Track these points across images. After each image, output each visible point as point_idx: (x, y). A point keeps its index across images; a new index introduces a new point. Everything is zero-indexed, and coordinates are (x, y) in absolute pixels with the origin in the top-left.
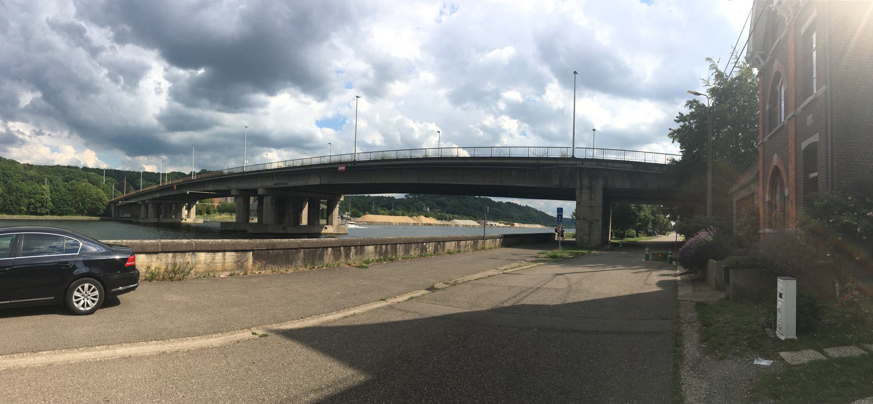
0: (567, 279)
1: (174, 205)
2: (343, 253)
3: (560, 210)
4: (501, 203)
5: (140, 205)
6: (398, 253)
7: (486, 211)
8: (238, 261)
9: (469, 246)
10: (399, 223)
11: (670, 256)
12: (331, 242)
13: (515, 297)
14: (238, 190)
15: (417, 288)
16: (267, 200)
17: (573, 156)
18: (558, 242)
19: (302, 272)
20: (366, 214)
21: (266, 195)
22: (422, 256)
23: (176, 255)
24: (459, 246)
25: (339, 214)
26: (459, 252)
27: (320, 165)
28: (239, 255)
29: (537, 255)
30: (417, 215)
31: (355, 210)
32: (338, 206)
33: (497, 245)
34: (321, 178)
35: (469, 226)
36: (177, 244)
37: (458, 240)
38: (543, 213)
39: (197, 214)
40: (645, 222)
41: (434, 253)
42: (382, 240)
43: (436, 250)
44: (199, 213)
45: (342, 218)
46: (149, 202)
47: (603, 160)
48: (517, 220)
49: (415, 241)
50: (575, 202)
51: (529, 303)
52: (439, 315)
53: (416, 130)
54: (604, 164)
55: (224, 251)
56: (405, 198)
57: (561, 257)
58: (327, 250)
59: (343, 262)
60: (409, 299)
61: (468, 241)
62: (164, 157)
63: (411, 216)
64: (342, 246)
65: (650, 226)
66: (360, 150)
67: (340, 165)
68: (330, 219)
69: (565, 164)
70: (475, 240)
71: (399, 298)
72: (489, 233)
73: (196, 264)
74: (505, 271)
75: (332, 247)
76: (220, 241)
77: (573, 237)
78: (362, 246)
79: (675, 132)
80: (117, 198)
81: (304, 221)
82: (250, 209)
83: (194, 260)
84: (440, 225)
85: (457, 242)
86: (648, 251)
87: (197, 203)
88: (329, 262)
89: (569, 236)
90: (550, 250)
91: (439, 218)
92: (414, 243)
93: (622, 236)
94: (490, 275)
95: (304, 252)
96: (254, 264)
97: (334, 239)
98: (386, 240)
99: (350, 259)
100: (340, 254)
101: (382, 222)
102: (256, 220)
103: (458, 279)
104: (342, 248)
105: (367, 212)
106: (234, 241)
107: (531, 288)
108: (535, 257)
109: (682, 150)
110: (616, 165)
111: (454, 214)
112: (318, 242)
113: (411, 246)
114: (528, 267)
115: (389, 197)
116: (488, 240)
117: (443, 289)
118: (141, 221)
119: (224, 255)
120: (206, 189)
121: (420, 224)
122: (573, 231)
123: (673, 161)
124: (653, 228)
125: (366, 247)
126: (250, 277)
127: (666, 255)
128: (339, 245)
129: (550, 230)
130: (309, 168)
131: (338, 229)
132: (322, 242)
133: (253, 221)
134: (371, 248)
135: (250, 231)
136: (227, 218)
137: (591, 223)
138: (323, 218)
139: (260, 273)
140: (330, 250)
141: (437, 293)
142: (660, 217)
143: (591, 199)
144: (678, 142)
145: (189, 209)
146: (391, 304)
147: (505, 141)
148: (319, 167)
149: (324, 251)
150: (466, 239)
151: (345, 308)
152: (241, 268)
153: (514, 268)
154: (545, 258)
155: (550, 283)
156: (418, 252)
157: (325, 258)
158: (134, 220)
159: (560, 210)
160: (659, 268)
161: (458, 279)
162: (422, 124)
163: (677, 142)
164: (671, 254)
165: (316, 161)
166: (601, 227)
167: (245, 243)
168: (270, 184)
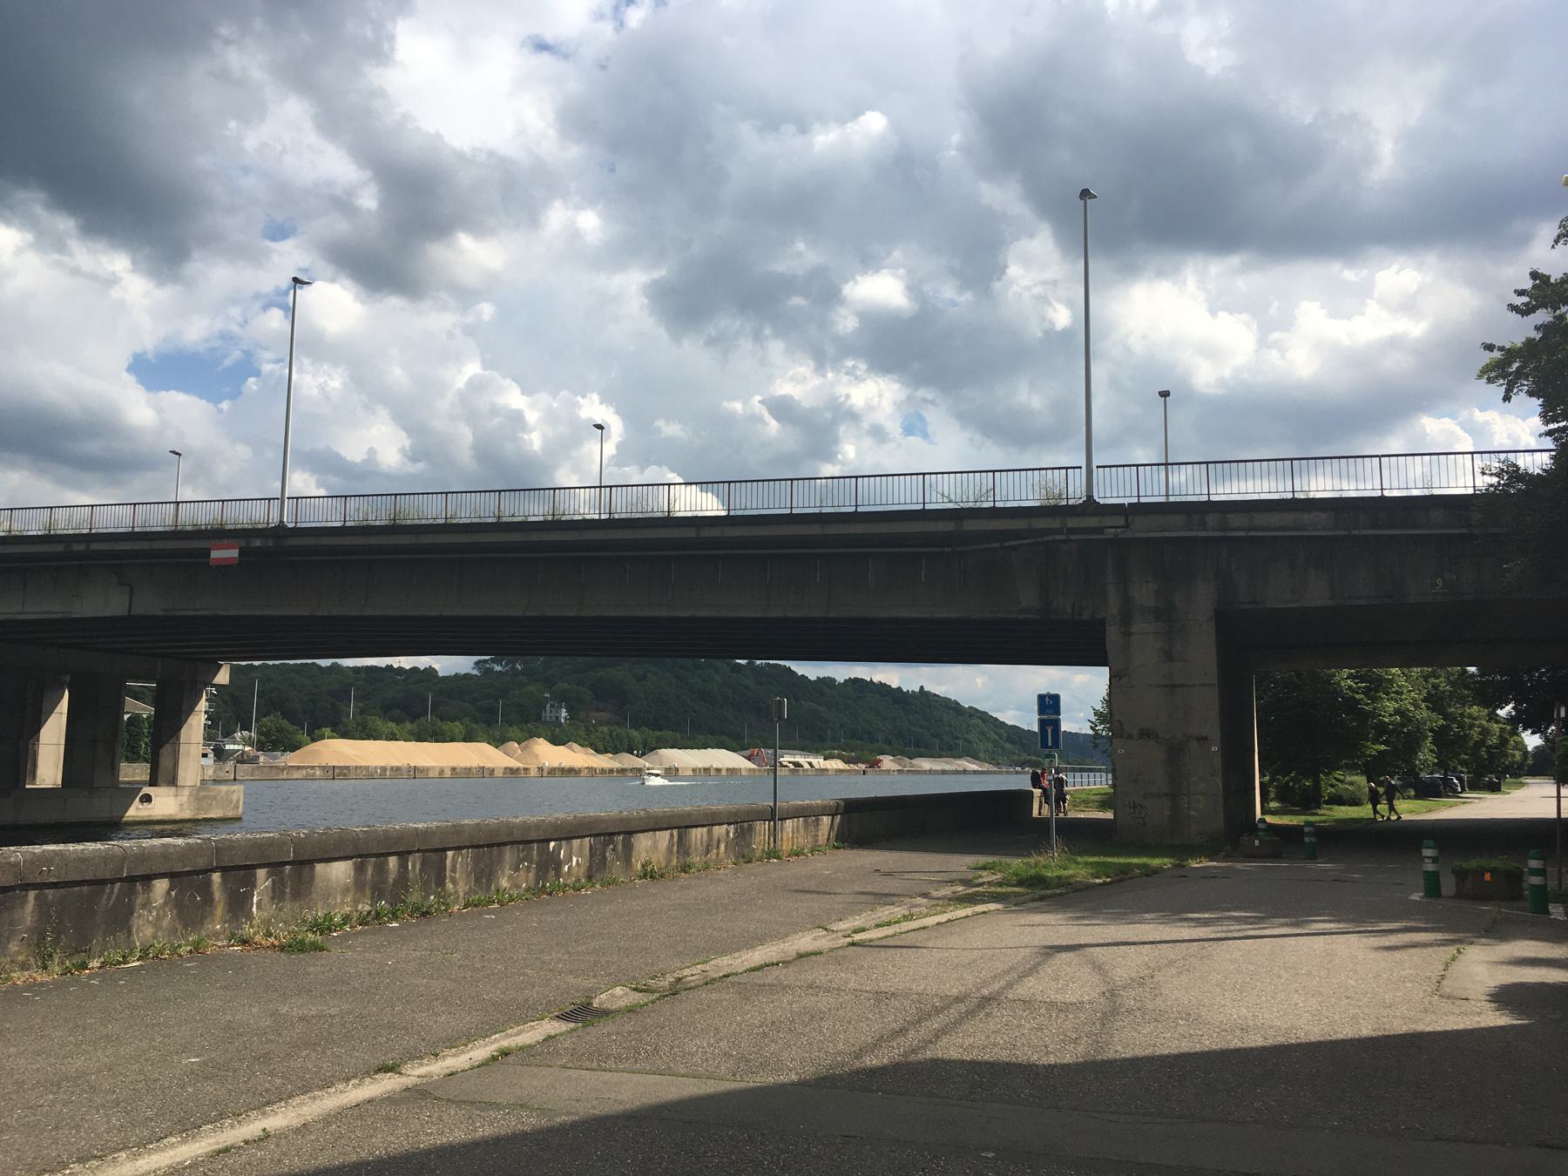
0: (1097, 967)
2: (218, 894)
3: (1049, 705)
4: (828, 682)
6: (450, 886)
7: (781, 717)
9: (722, 846)
10: (454, 769)
11: (1535, 880)
12: (165, 854)
13: (903, 1031)
15: (523, 1014)
17: (1090, 497)
18: (1043, 823)
19: (29, 987)
20: (322, 737)
22: (543, 890)
24: (683, 846)
25: (209, 737)
26: (685, 868)
27: (131, 536)
29: (970, 876)
30: (519, 734)
31: (273, 721)
32: (203, 705)
33: (822, 839)
34: (131, 590)
35: (718, 770)
37: (681, 825)
38: (984, 717)
40: (1405, 739)
41: (589, 878)
42: (387, 837)
43: (596, 867)
45: (220, 754)
47: (1209, 502)
48: (890, 744)
49: (518, 836)
50: (1104, 672)
51: (954, 1054)
52: (619, 1108)
53: (532, 417)
54: (1211, 519)
56: (475, 672)
57: (1061, 882)
58: (148, 888)
59: (216, 935)
60: (494, 1058)
61: (716, 828)
63: (498, 742)
64: (214, 870)
65: (1426, 754)
66: (319, 485)
68: (165, 761)
69: (1059, 531)
70: (743, 821)
71: (454, 1055)
72: (791, 798)
74: (857, 937)
75: (172, 875)
77: (1104, 805)
79: (1510, 354)
81: (49, 769)
84: (611, 771)
85: (675, 832)
86: (1434, 860)
88: (155, 937)
89: (1086, 802)
90: (1019, 855)
91: (602, 747)
93: (1310, 801)
94: (803, 950)
95: (41, 903)
97: (180, 841)
98: (401, 836)
99: (250, 917)
100: (208, 899)
101: (384, 769)
103: (686, 972)
104: (216, 877)
105: (327, 731)
107: (958, 999)
108: (966, 883)
109: (1552, 426)
110: (1260, 519)
111: (660, 729)
112: (106, 858)
113: (500, 854)
114: (943, 918)
115: (415, 670)
116: (789, 823)
117: (631, 1010)
121: (533, 773)
122: (1100, 783)
123: (1514, 474)
124: (1441, 765)
125: (319, 867)
127: (1515, 878)
128: (201, 863)
129: (1019, 781)
131: (198, 799)
132: (125, 857)
134: (339, 872)
137: (1175, 752)
138: (134, 757)
140: (161, 886)
141: (605, 1028)
142: (1470, 716)
143: (1169, 657)
144: (1531, 394)
146: (419, 1081)
147: (852, 453)
148: (127, 546)
149: (132, 893)
150: (711, 820)
151: (221, 1116)
153: (889, 924)
154: (1000, 884)
155: (1031, 982)
156: (526, 879)
157: (136, 922)
159: (1049, 705)
160: (1496, 931)
161: (686, 972)
162: (554, 395)
163: (1523, 394)
164: (1540, 872)
165: (114, 520)
166: (1218, 762)
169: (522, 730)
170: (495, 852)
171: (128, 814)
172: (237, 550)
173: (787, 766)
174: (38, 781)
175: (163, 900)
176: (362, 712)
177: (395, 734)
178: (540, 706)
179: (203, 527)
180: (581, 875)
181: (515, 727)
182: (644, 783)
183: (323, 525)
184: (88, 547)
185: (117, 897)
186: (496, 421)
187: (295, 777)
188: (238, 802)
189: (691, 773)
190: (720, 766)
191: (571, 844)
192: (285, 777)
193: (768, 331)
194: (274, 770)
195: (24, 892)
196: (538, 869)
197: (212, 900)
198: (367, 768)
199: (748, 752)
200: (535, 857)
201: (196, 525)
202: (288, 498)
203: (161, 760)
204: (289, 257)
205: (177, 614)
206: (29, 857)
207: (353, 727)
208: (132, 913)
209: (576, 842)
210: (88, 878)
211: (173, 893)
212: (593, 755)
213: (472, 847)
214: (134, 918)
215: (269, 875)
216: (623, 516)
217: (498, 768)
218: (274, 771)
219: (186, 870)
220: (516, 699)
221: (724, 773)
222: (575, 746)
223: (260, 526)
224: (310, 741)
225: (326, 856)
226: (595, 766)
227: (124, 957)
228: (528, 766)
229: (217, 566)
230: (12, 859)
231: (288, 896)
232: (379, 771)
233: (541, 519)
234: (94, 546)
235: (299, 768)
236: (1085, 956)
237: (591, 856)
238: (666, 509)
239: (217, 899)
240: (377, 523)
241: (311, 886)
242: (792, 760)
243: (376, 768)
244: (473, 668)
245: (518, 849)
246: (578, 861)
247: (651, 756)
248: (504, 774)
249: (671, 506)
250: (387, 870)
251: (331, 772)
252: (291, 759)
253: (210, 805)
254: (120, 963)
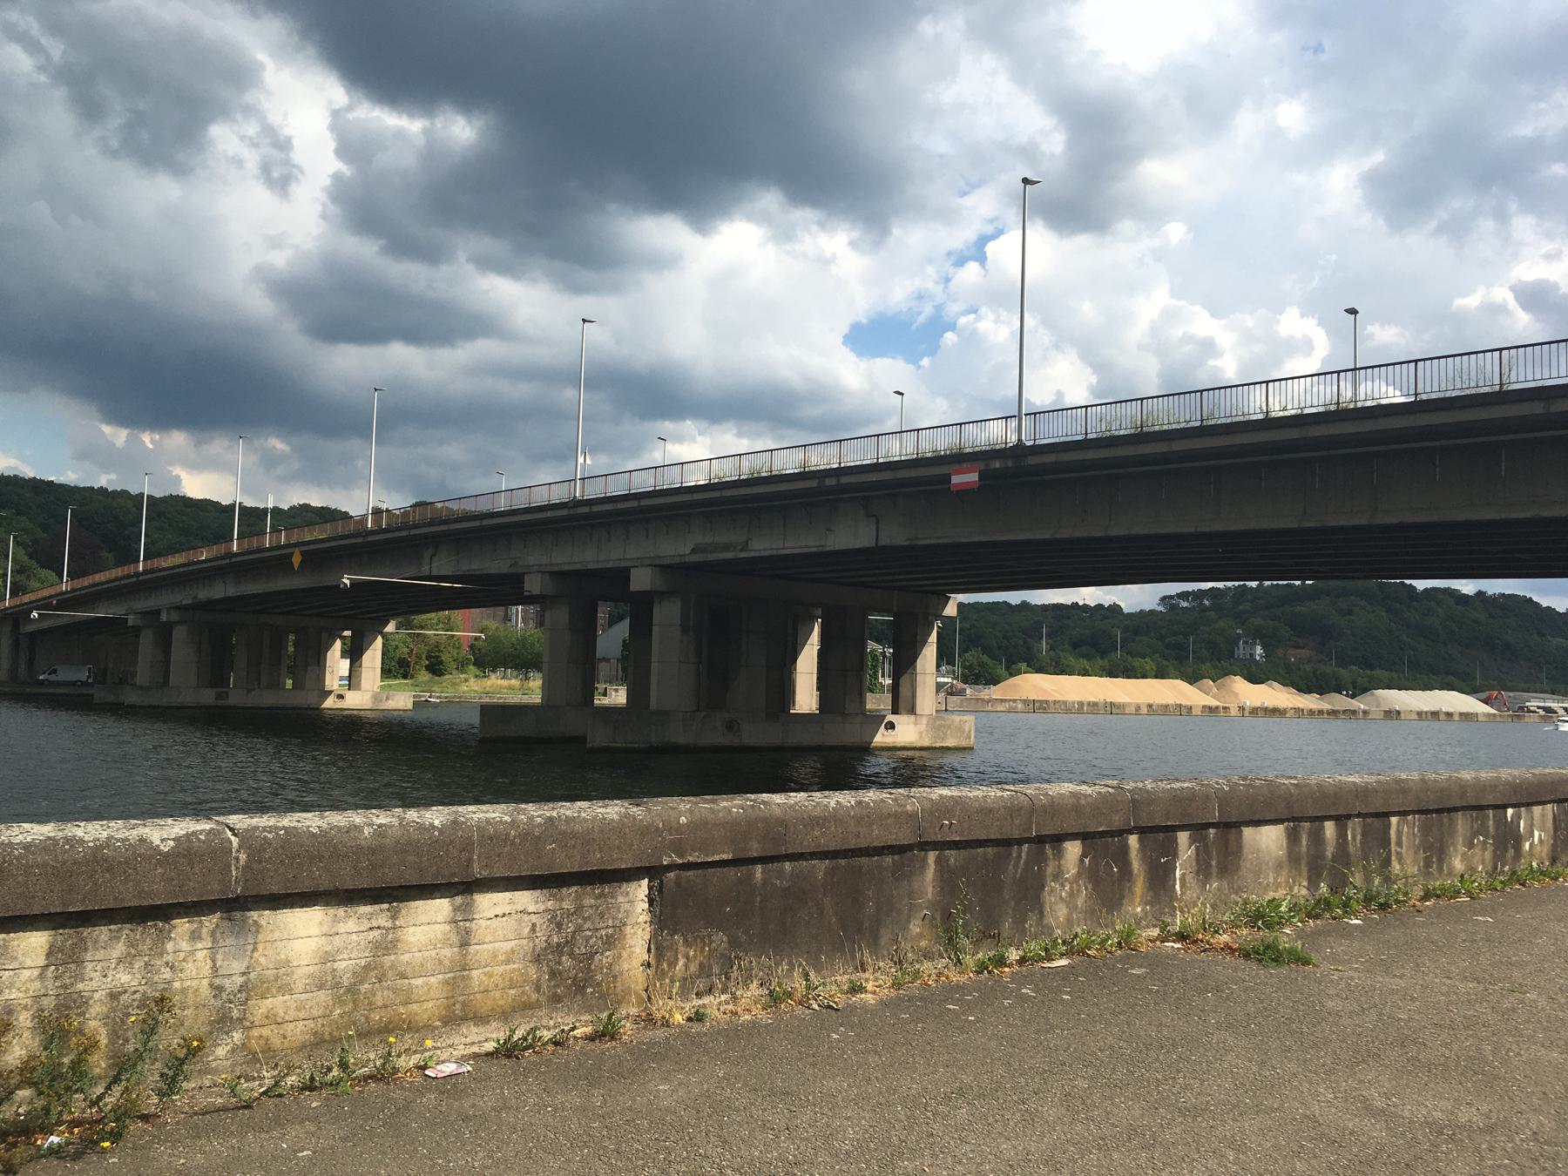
1: (292, 637)
2: (1136, 865)
5: (137, 630)
8: (559, 949)
10: (1150, 706)
14: (551, 573)
16: (666, 615)
21: (662, 595)
23: (82, 945)
28: (566, 905)
32: (933, 637)
34: (878, 522)
35: (1449, 715)
36: (100, 858)
39: (387, 672)
44: (396, 668)
46: (175, 617)
55: (465, 887)
56: (1161, 608)
58: (1059, 854)
62: (278, 444)
63: (1192, 679)
64: (1130, 832)
67: (957, 467)
68: (904, 690)
73: (248, 990)
75: (1084, 837)
76: (436, 816)
78: (1230, 827)
80: (27, 598)
81: (806, 698)
82: (598, 655)
83: (238, 966)
84: (1321, 712)
87: (390, 627)
92: (1465, 808)
95: (946, 877)
96: (660, 957)
101: (1081, 704)
102: (618, 697)
104: (1133, 840)
106: (536, 813)
113: (1452, 822)
118: (132, 698)
119: (464, 915)
120: (425, 570)
121: (1234, 711)
125: (1247, 832)
126: (647, 1056)
128: (1117, 821)
130: (830, 482)
133: (605, 701)
134: (1268, 840)
135: (599, 737)
136: (507, 688)
139: (698, 1017)
140: (1073, 849)
145: (354, 653)
149: (1038, 859)
152: (579, 987)
156: (1482, 859)
157: (1049, 899)
158: (100, 694)
167: (606, 826)
168: (678, 547)
169: (1215, 667)
170: (1445, 820)
171: (875, 740)
172: (977, 474)
173: (1535, 712)
174: (797, 707)
175: (1077, 869)
176: (1052, 648)
177: (1087, 671)
178: (1234, 642)
179: (943, 453)
180: (1545, 857)
181: (1208, 664)
182: (1557, 729)
183: (1062, 439)
184: (838, 481)
185: (1026, 863)
186: (1187, 348)
187: (999, 709)
188: (970, 732)
189: (1416, 717)
190: (1451, 710)
191: (1532, 812)
192: (990, 708)
193: (1513, 206)
194: (980, 701)
195: (923, 853)
196: (1496, 846)
197: (1130, 873)
198: (1065, 703)
199: (1485, 695)
200: (1491, 830)
201: (936, 451)
202: (1025, 415)
203: (900, 689)
204: (983, 205)
205: (920, 543)
206: (927, 805)
207: (1047, 663)
208: (1043, 887)
209: (1537, 810)
210: (993, 837)
211: (1087, 861)
212: (1296, 694)
213: (1419, 812)
214: (1046, 894)
215: (1192, 840)
216: (1434, 396)
217: (1197, 706)
218: (980, 703)
219: (1101, 829)
220: (1207, 635)
221: (1456, 717)
222: (1275, 684)
223: (998, 447)
224: (1008, 676)
225: (1256, 818)
226: (1301, 706)
227: (1046, 950)
228: (1227, 705)
229: (957, 491)
230: (909, 808)
231: (1214, 871)
232: (1077, 706)
233: (1321, 409)
234: (844, 480)
235: (1002, 701)
236: (1201, 834)
237: (1556, 829)
238: (1497, 381)
239: (1136, 871)
240: (1122, 433)
241: (1240, 857)
242: (1542, 704)
243: (1073, 703)
244: (1159, 605)
245: (1472, 816)
246: (1540, 836)
247: (1367, 697)
248: (1202, 712)
249: (1505, 378)
250: (1324, 838)
251: (1031, 706)
252: (994, 692)
253: (945, 734)
254: (1042, 959)
